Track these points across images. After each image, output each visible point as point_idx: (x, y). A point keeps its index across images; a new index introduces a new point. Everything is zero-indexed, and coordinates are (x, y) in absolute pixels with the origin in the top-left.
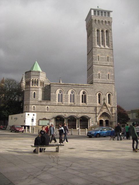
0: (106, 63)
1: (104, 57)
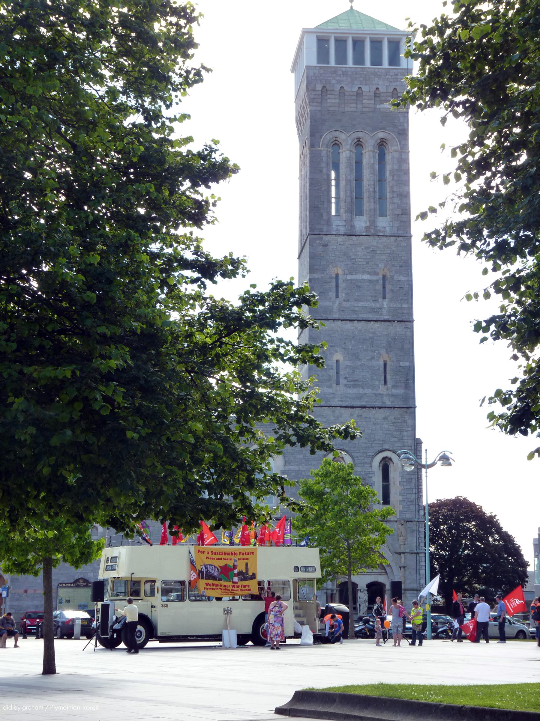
0: (373, 310)
1: (366, 277)
